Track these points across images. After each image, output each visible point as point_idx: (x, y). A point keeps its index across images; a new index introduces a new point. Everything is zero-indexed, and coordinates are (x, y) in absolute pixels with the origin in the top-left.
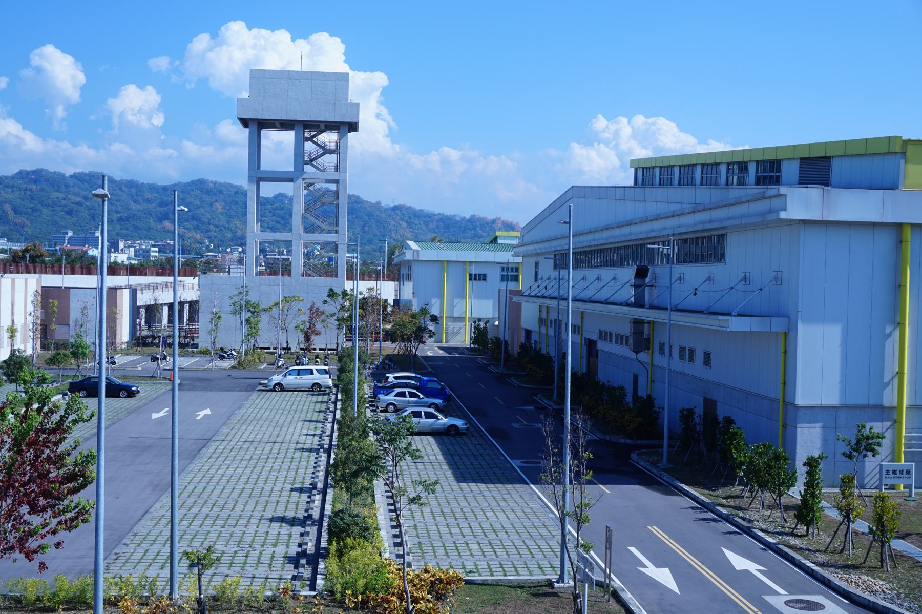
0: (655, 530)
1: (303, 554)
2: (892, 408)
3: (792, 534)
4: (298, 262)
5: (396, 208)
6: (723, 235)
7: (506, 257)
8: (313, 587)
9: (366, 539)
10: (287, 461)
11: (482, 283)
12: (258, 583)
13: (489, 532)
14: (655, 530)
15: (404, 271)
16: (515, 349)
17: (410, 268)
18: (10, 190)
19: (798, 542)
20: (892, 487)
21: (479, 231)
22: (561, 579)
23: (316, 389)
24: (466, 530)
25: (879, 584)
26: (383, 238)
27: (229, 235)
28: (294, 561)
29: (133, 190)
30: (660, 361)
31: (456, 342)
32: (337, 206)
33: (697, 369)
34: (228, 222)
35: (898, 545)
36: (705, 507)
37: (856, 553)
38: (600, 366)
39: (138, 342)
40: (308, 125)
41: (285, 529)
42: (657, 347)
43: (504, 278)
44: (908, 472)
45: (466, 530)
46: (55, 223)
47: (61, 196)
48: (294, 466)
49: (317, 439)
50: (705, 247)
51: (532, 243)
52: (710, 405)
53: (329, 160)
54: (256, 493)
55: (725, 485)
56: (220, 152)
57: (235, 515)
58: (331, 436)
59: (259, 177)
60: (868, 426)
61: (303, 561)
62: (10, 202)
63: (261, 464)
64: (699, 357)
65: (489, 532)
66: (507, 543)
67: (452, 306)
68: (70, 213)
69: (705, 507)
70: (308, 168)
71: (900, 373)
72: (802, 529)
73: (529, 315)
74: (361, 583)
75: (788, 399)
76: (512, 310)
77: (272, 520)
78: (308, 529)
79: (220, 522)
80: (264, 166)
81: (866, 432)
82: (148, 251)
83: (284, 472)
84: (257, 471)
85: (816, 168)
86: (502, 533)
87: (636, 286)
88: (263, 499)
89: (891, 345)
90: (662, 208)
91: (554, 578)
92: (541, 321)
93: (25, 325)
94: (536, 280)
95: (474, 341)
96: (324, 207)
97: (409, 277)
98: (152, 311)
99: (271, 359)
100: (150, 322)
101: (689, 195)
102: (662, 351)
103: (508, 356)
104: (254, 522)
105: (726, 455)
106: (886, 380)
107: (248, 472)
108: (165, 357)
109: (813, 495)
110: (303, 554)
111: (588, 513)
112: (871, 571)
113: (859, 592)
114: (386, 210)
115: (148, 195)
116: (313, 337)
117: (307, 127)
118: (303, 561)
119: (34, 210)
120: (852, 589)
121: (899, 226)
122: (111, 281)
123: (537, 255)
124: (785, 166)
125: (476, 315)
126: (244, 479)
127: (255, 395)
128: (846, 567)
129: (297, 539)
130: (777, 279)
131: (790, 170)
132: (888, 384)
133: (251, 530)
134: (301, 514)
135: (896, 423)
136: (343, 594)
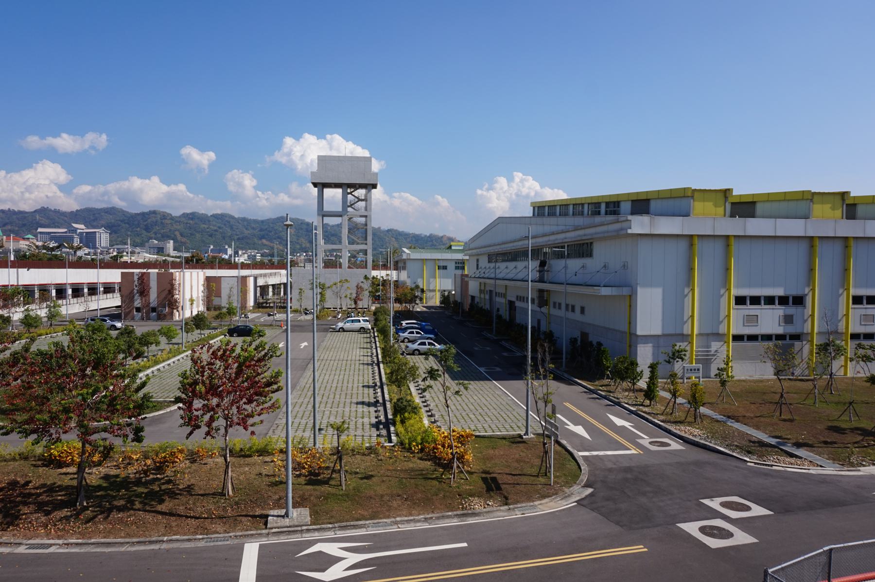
0: (568, 405)
1: (379, 423)
2: (688, 335)
3: (642, 405)
4: (344, 261)
5: (389, 231)
6: (591, 243)
7: (460, 256)
8: (390, 441)
9: (416, 414)
10: (357, 371)
11: (444, 271)
12: (359, 439)
13: (478, 408)
14: (568, 405)
15: (400, 265)
16: (467, 307)
17: (405, 263)
19: (646, 409)
20: (688, 378)
21: (446, 244)
22: (527, 433)
23: (362, 330)
24: (465, 407)
25: (696, 432)
26: (389, 247)
27: (298, 247)
28: (376, 426)
29: (245, 223)
30: (554, 312)
31: (431, 303)
32: (366, 230)
33: (577, 316)
35: (703, 410)
36: (591, 391)
37: (679, 415)
38: (518, 316)
39: (258, 306)
40: (350, 186)
41: (366, 409)
42: (552, 305)
43: (457, 268)
44: (698, 370)
45: (465, 407)
46: (203, 241)
47: (206, 226)
48: (361, 373)
49: (369, 358)
50: (583, 249)
51: (475, 249)
52: (584, 335)
53: (362, 204)
54: (344, 388)
55: (599, 379)
56: (299, 201)
57: (336, 401)
58: (377, 356)
59: (323, 214)
60: (678, 344)
61: (381, 427)
63: (342, 373)
64: (578, 310)
65: (478, 408)
66: (490, 414)
67: (429, 283)
68: (211, 236)
69: (591, 391)
70: (349, 209)
71: (692, 316)
72: (647, 402)
73: (473, 287)
74: (419, 438)
75: (633, 332)
76: (463, 283)
77: (357, 403)
78: (379, 408)
79: (329, 405)
80: (325, 209)
81: (677, 348)
82: (255, 256)
83: (356, 376)
84: (341, 377)
85: (641, 205)
86: (485, 408)
87: (540, 271)
88: (349, 392)
89: (688, 301)
90: (554, 228)
91: (522, 433)
92: (481, 291)
93: (198, 297)
94: (477, 268)
95: (441, 303)
96: (359, 232)
97: (404, 268)
98: (264, 289)
99: (333, 314)
100: (262, 295)
101: (570, 221)
102: (554, 307)
103: (463, 310)
104: (348, 405)
105: (599, 363)
107: (337, 377)
109: (653, 384)
110: (379, 423)
111: (551, 397)
112: (690, 424)
113: (686, 435)
114: (384, 232)
115: (253, 225)
116: (359, 302)
117: (348, 187)
118: (381, 427)
119: (191, 234)
120: (683, 434)
122: (245, 272)
123: (478, 255)
124: (622, 205)
125: (443, 288)
126: (335, 381)
127: (329, 334)
128: (676, 422)
129: (373, 415)
130: (625, 267)
131: (626, 207)
133: (347, 409)
134: (373, 400)
135: (691, 343)
136: (410, 444)
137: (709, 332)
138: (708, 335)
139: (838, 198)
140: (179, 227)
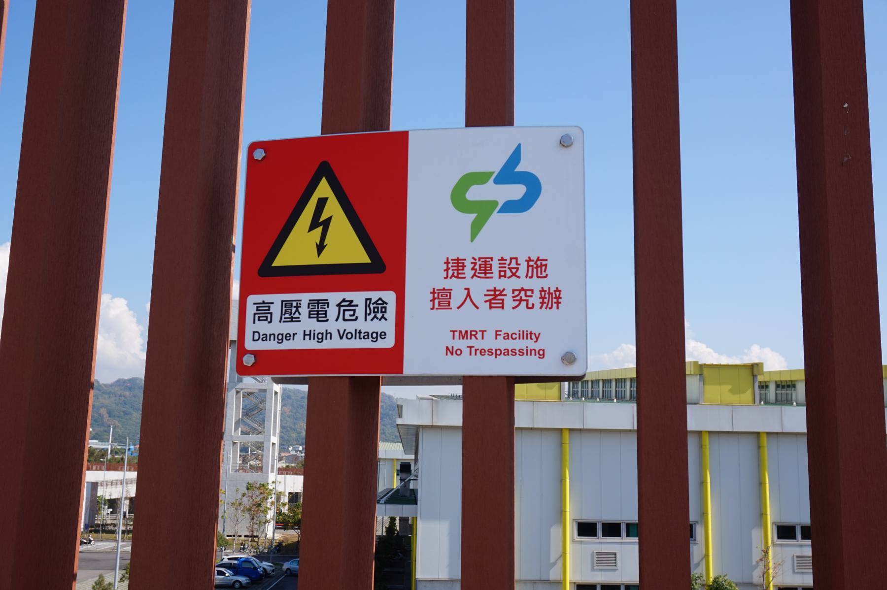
18: (107, 396)
34: (295, 424)
62: (106, 407)
71: (707, 556)
80: (518, 387)
106: (552, 560)
108: (90, 541)
119: (125, 413)
121: (758, 433)
132: (555, 563)
137: (535, 577)
138: (534, 582)
139: (746, 374)
140: (106, 402)
